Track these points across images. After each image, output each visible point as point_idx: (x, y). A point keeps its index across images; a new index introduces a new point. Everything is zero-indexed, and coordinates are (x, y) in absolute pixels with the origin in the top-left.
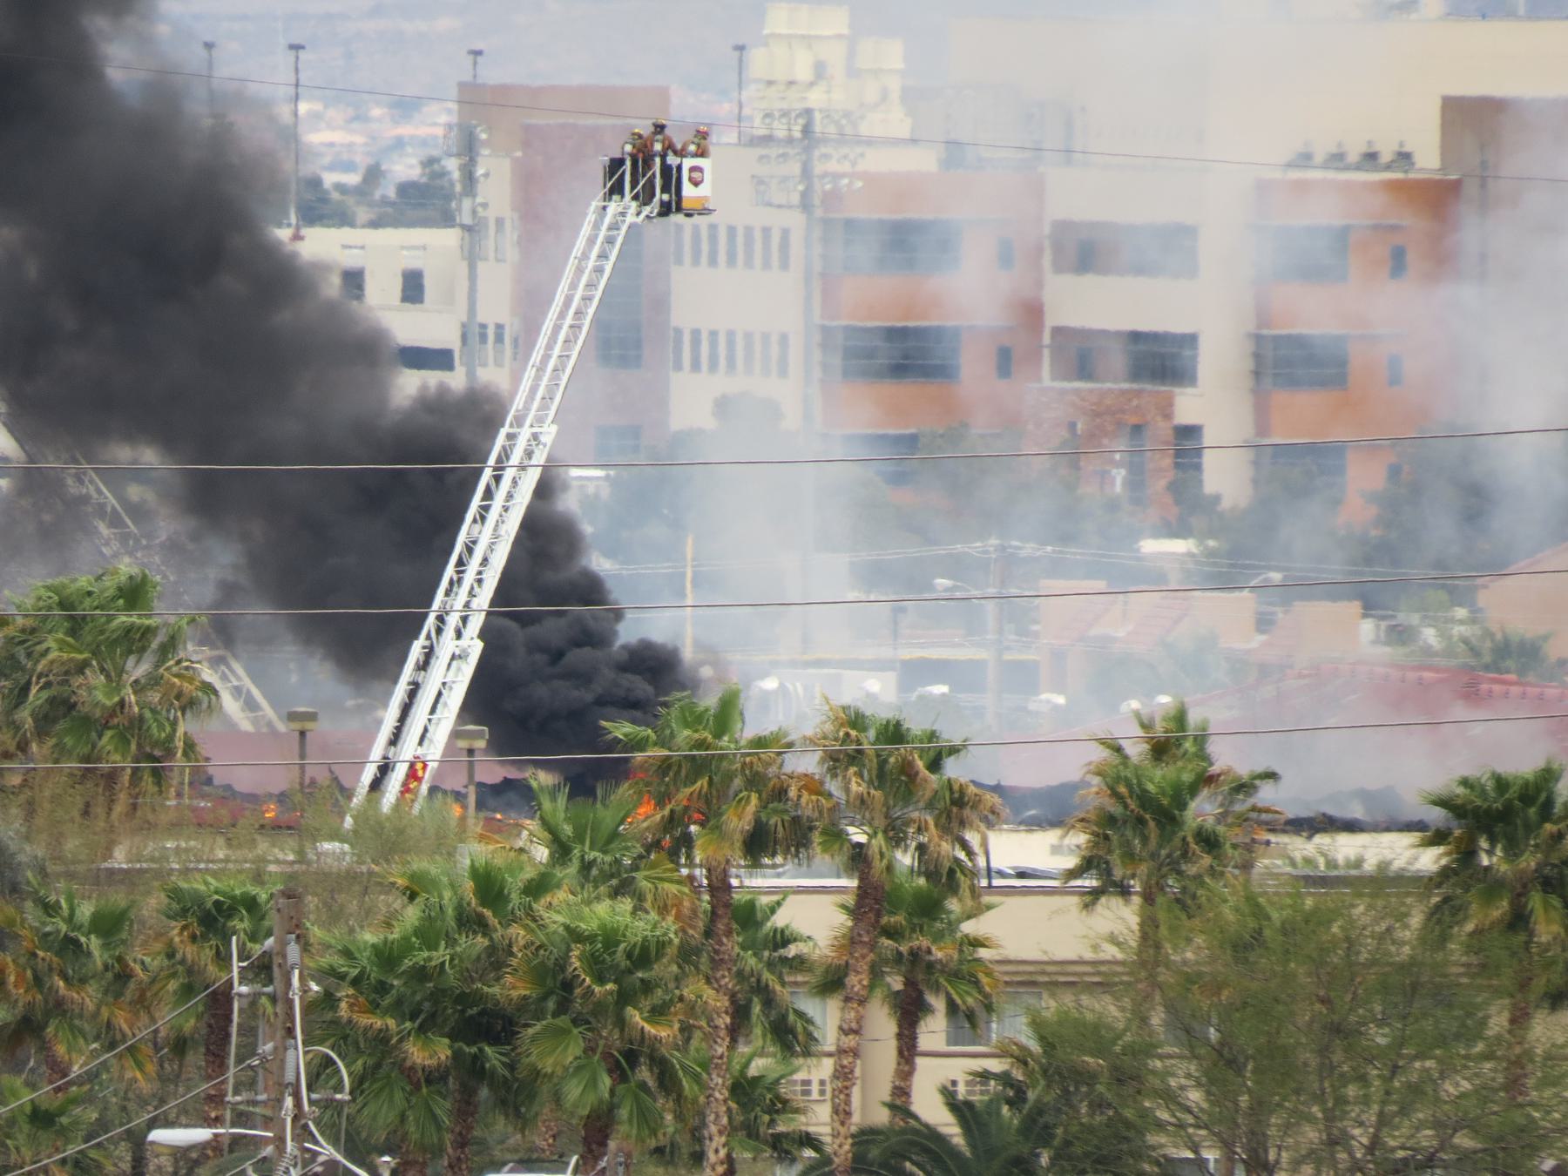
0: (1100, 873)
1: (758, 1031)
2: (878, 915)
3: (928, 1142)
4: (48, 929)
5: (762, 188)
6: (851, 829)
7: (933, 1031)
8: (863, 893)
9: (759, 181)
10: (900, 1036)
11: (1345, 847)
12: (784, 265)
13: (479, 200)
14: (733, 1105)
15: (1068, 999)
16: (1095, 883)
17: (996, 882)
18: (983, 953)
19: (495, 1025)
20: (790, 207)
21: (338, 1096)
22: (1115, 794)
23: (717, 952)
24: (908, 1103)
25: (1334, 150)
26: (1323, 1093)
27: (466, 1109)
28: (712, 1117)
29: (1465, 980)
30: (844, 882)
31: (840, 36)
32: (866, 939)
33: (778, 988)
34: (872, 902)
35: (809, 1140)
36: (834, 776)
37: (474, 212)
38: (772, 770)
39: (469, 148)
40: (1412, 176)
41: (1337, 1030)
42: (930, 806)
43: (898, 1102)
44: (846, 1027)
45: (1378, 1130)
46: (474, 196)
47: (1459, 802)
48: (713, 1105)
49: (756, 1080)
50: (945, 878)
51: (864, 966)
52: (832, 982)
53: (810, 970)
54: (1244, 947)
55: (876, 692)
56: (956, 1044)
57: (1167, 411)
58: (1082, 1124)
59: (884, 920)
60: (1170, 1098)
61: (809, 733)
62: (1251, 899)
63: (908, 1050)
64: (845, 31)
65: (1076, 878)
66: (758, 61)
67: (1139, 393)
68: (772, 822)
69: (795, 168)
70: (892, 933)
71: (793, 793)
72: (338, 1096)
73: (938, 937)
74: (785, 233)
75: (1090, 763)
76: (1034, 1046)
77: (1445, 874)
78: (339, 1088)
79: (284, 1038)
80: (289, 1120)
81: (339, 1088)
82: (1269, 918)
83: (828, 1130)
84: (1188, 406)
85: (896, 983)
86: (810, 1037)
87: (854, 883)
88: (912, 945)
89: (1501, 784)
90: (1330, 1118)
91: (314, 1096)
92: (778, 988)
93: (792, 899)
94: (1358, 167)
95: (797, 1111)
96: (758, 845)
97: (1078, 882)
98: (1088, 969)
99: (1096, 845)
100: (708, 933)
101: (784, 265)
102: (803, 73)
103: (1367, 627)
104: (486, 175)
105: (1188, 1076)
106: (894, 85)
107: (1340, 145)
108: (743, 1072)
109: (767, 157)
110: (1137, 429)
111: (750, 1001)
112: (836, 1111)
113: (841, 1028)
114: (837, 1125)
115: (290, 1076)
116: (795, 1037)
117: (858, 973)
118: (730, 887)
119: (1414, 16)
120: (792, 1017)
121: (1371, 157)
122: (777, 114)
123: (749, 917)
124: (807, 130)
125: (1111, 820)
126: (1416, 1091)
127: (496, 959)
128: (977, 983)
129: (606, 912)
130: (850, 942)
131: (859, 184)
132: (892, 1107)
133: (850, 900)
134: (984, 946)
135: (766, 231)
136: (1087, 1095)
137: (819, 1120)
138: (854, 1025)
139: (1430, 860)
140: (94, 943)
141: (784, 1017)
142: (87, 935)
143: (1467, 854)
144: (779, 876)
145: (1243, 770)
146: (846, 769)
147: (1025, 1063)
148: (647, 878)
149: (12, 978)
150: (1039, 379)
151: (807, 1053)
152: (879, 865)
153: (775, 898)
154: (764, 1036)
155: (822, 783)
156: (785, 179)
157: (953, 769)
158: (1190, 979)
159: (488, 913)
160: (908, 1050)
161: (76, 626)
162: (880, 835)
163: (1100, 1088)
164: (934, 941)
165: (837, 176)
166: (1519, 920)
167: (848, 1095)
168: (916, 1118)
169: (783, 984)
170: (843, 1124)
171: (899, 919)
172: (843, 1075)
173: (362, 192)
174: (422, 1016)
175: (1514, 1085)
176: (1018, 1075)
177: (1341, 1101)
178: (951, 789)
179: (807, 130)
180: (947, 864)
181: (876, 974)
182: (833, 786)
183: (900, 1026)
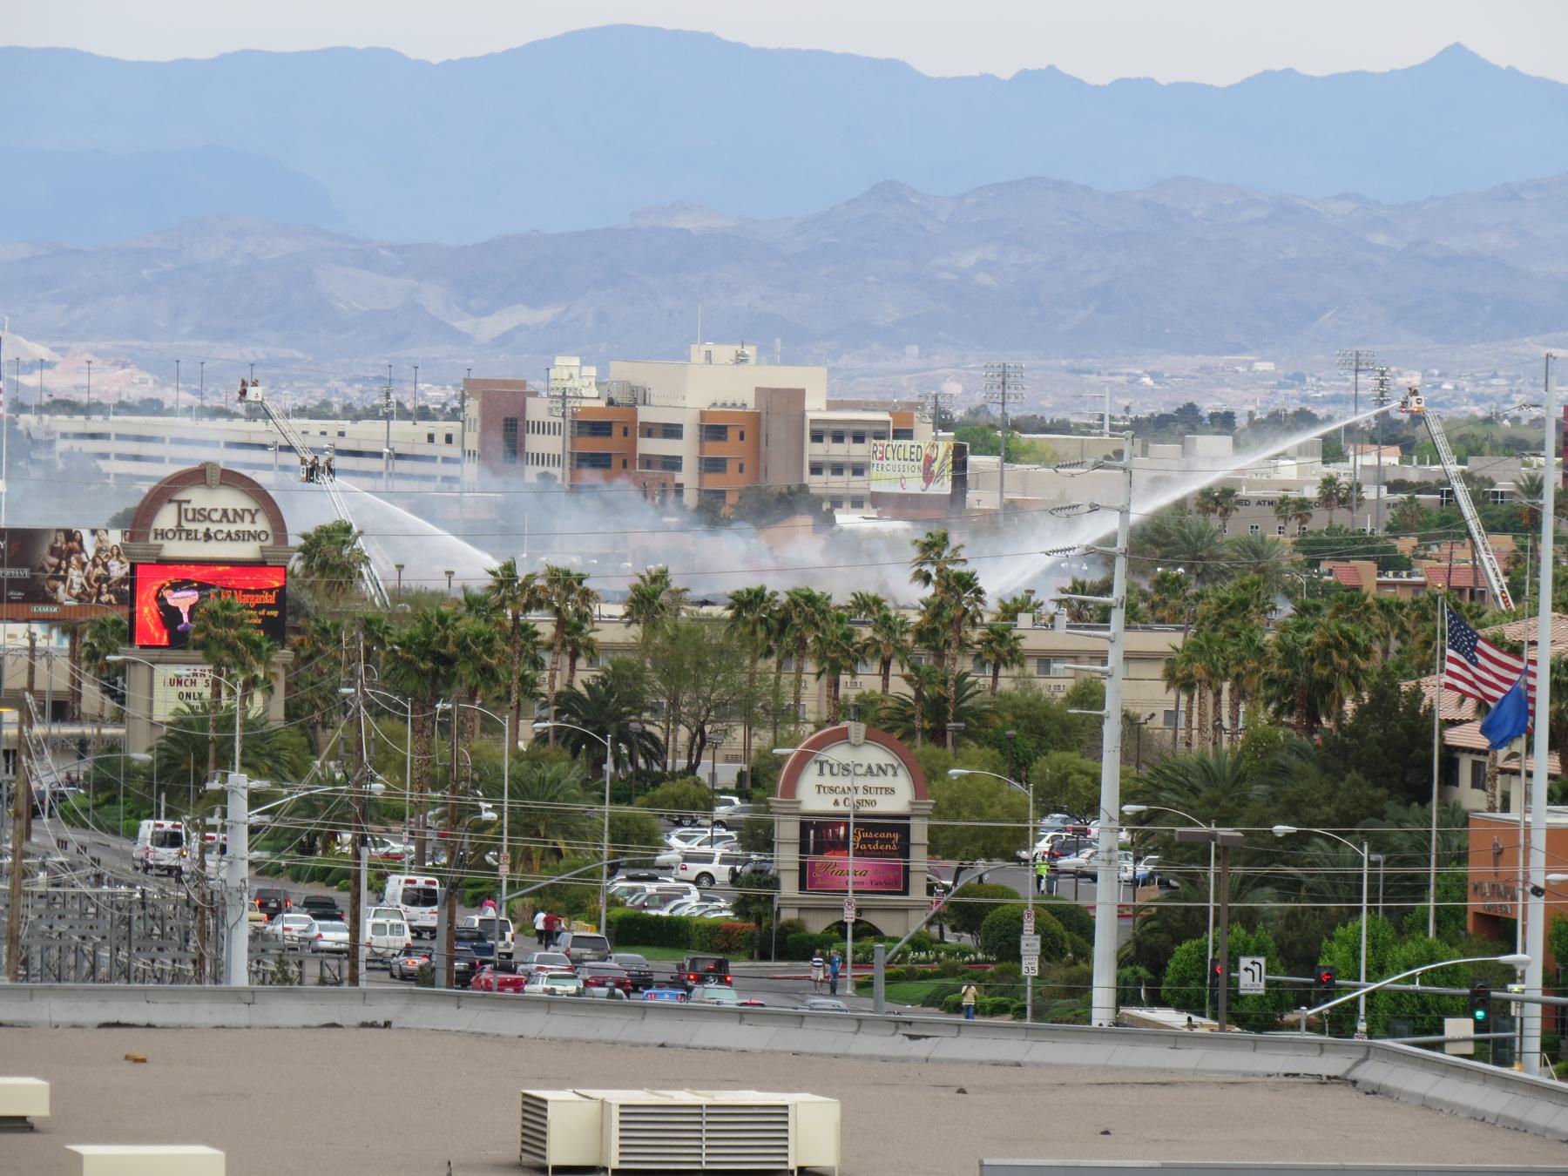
0: (630, 618)
3: (577, 697)
7: (581, 663)
19: (448, 661)
27: (434, 684)
34: (562, 624)
35: (542, 695)
39: (463, 398)
50: (584, 617)
54: (673, 639)
63: (573, 668)
66: (552, 372)
84: (680, 477)
85: (569, 649)
88: (573, 637)
89: (749, 592)
96: (527, 608)
106: (593, 380)
110: (664, 485)
121: (734, 405)
127: (445, 640)
130: (556, 636)
136: (1506, 719)
137: (545, 689)
139: (728, 614)
143: (739, 613)
157: (585, 583)
160: (573, 668)
161: (330, 538)
166: (754, 633)
172: (553, 676)
173: (441, 411)
175: (751, 680)
181: (564, 645)
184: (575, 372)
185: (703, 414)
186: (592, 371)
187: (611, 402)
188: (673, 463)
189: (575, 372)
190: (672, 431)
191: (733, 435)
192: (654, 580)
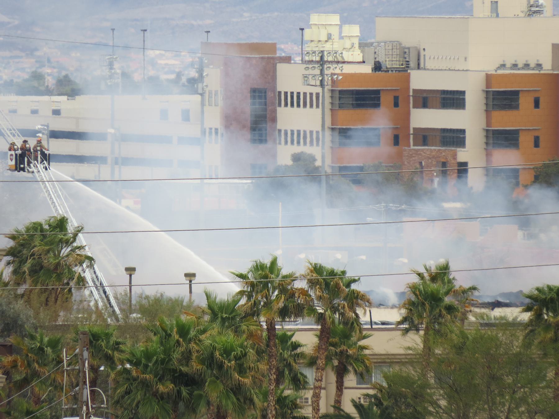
0: (410, 323)
1: (287, 381)
2: (328, 338)
4: (33, 346)
5: (306, 79)
6: (318, 308)
7: (350, 380)
8: (322, 331)
9: (305, 77)
10: (337, 382)
11: (498, 312)
12: (318, 106)
13: (205, 84)
14: (277, 407)
15: (397, 368)
16: (407, 326)
17: (374, 326)
18: (367, 352)
20: (316, 86)
21: (102, 406)
22: (414, 293)
23: (270, 352)
24: (340, 405)
25: (514, 63)
26: (488, 401)
28: (270, 411)
29: (537, 360)
30: (315, 327)
31: (337, 25)
32: (324, 347)
33: (294, 364)
34: (325, 334)
36: (312, 289)
37: (203, 89)
38: (289, 287)
40: (542, 72)
41: (493, 378)
42: (345, 299)
43: (337, 406)
44: (317, 379)
45: (508, 413)
46: (203, 83)
47: (535, 296)
48: (270, 407)
49: (286, 397)
51: (323, 357)
52: (312, 362)
53: (305, 358)
54: (459, 349)
55: (332, 260)
56: (360, 384)
57: (455, 156)
58: (402, 413)
59: (331, 340)
60: (435, 404)
61: (303, 273)
62: (462, 332)
64: (339, 23)
65: (401, 324)
66: (308, 35)
67: (444, 151)
68: (290, 305)
69: (317, 72)
70: (334, 345)
71: (297, 295)
72: (102, 406)
73: (350, 347)
74: (318, 94)
75: (408, 284)
76: (385, 384)
77: (531, 321)
78: (102, 402)
79: (83, 385)
80: (85, 415)
81: (102, 402)
82: (468, 338)
83: (311, 415)
84: (462, 155)
85: (336, 363)
86: (306, 382)
87: (319, 327)
90: (491, 410)
91: (94, 406)
92: (294, 364)
93: (297, 333)
94: (523, 68)
95: (301, 408)
96: (284, 313)
97: (402, 326)
98: (404, 357)
99: (408, 313)
100: (268, 346)
101: (318, 106)
102: (324, 38)
103: (520, 234)
104: (207, 75)
105: (440, 395)
106: (356, 41)
107: (516, 61)
108: (281, 396)
109: (308, 68)
111: (284, 370)
112: (314, 409)
113: (315, 379)
114: (314, 414)
115: (85, 399)
116: (300, 382)
117: (321, 359)
118: (275, 329)
119: (541, 16)
120: (299, 375)
122: (311, 52)
123: (285, 338)
124: (322, 57)
125: (412, 304)
126: (523, 400)
128: (363, 362)
129: (229, 337)
130: (318, 348)
131: (341, 77)
132: (334, 407)
133: (318, 333)
134: (366, 349)
135: (311, 94)
138: (320, 378)
139: (526, 317)
140: (49, 350)
141: (296, 375)
142: (46, 347)
143: (539, 316)
144: (297, 325)
145: (466, 286)
146: (316, 286)
147: (381, 391)
148: (244, 325)
149: (20, 364)
150: (409, 146)
151: (304, 388)
152: (329, 321)
153: (292, 333)
154: (289, 382)
155: (307, 291)
156: (314, 76)
157: (354, 286)
158: (441, 361)
159: (181, 340)
162: (329, 310)
163: (409, 400)
164: (349, 348)
165: (333, 74)
167: (318, 404)
168: (343, 411)
169: (296, 363)
170: (316, 413)
171: (336, 340)
172: (317, 396)
174: (159, 376)
176: (379, 395)
177: (494, 403)
178: (354, 293)
179: (322, 57)
180: (351, 320)
181: (329, 359)
182: (312, 293)
183: (337, 378)
184: (335, 32)
185: (489, 78)
186: (354, 30)
187: (378, 67)
188: (455, 138)
189: (335, 32)
190: (453, 100)
191: (525, 102)
192: (434, 278)
